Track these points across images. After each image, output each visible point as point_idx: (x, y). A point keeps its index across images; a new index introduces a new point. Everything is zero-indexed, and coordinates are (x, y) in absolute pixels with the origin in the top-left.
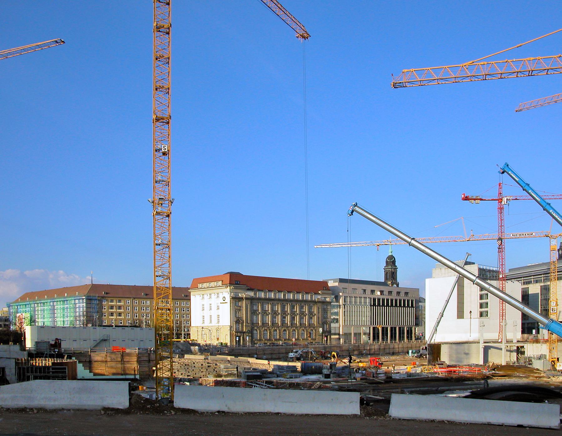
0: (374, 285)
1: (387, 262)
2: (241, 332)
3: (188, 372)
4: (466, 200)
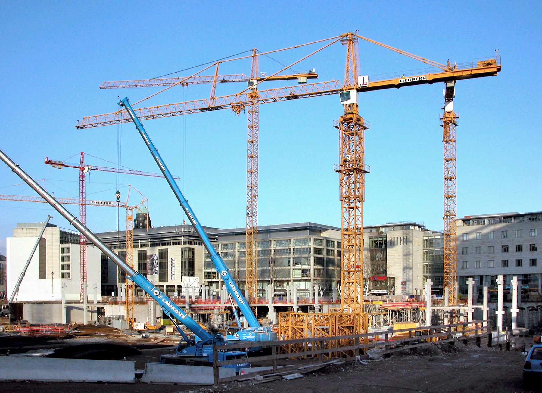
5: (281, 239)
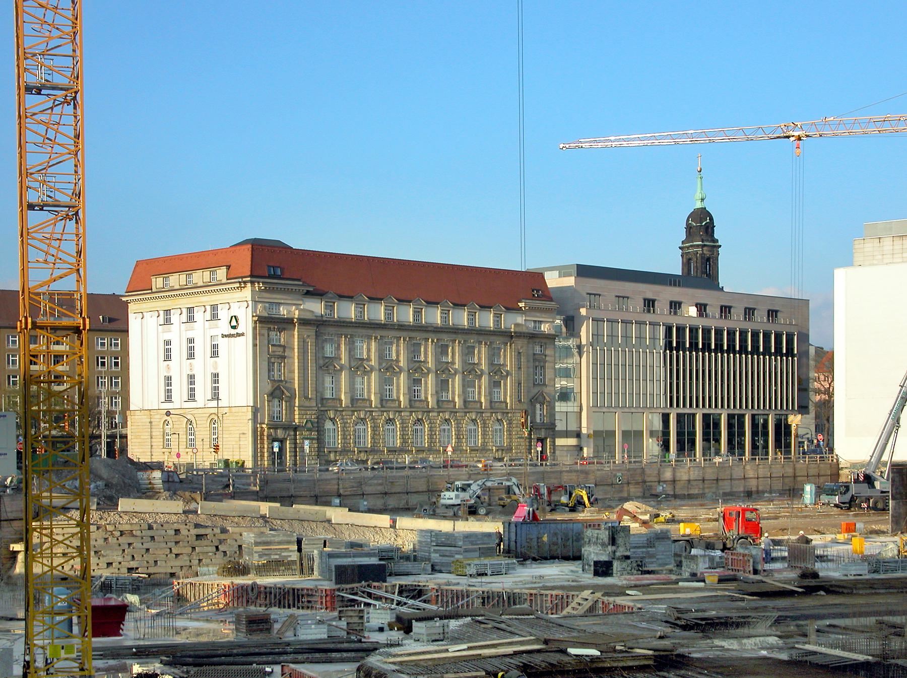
0: (679, 286)
1: (691, 228)
2: (286, 428)
3: (130, 558)
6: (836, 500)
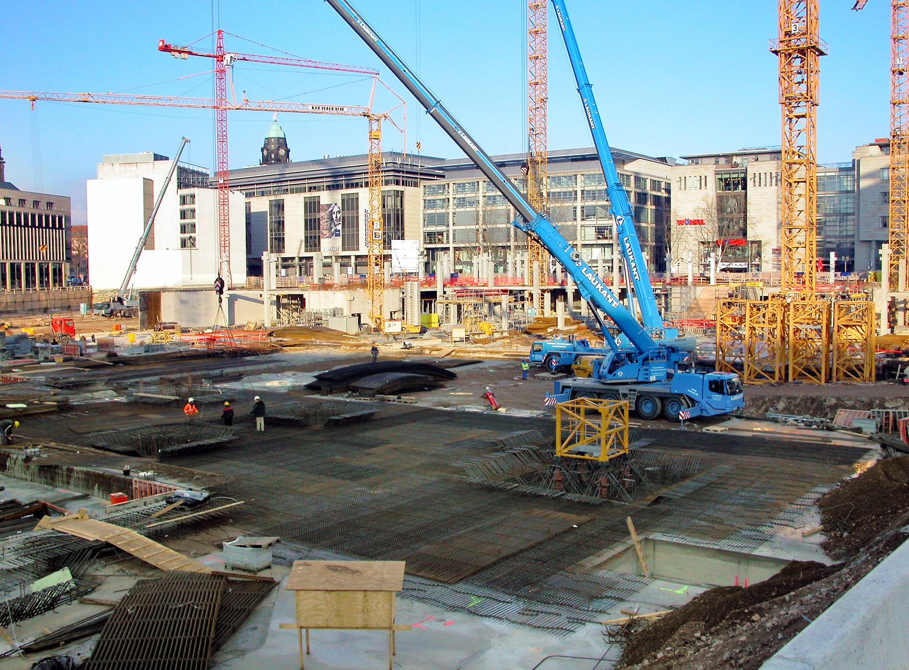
4: (165, 51)
5: (559, 175)
6: (103, 312)
